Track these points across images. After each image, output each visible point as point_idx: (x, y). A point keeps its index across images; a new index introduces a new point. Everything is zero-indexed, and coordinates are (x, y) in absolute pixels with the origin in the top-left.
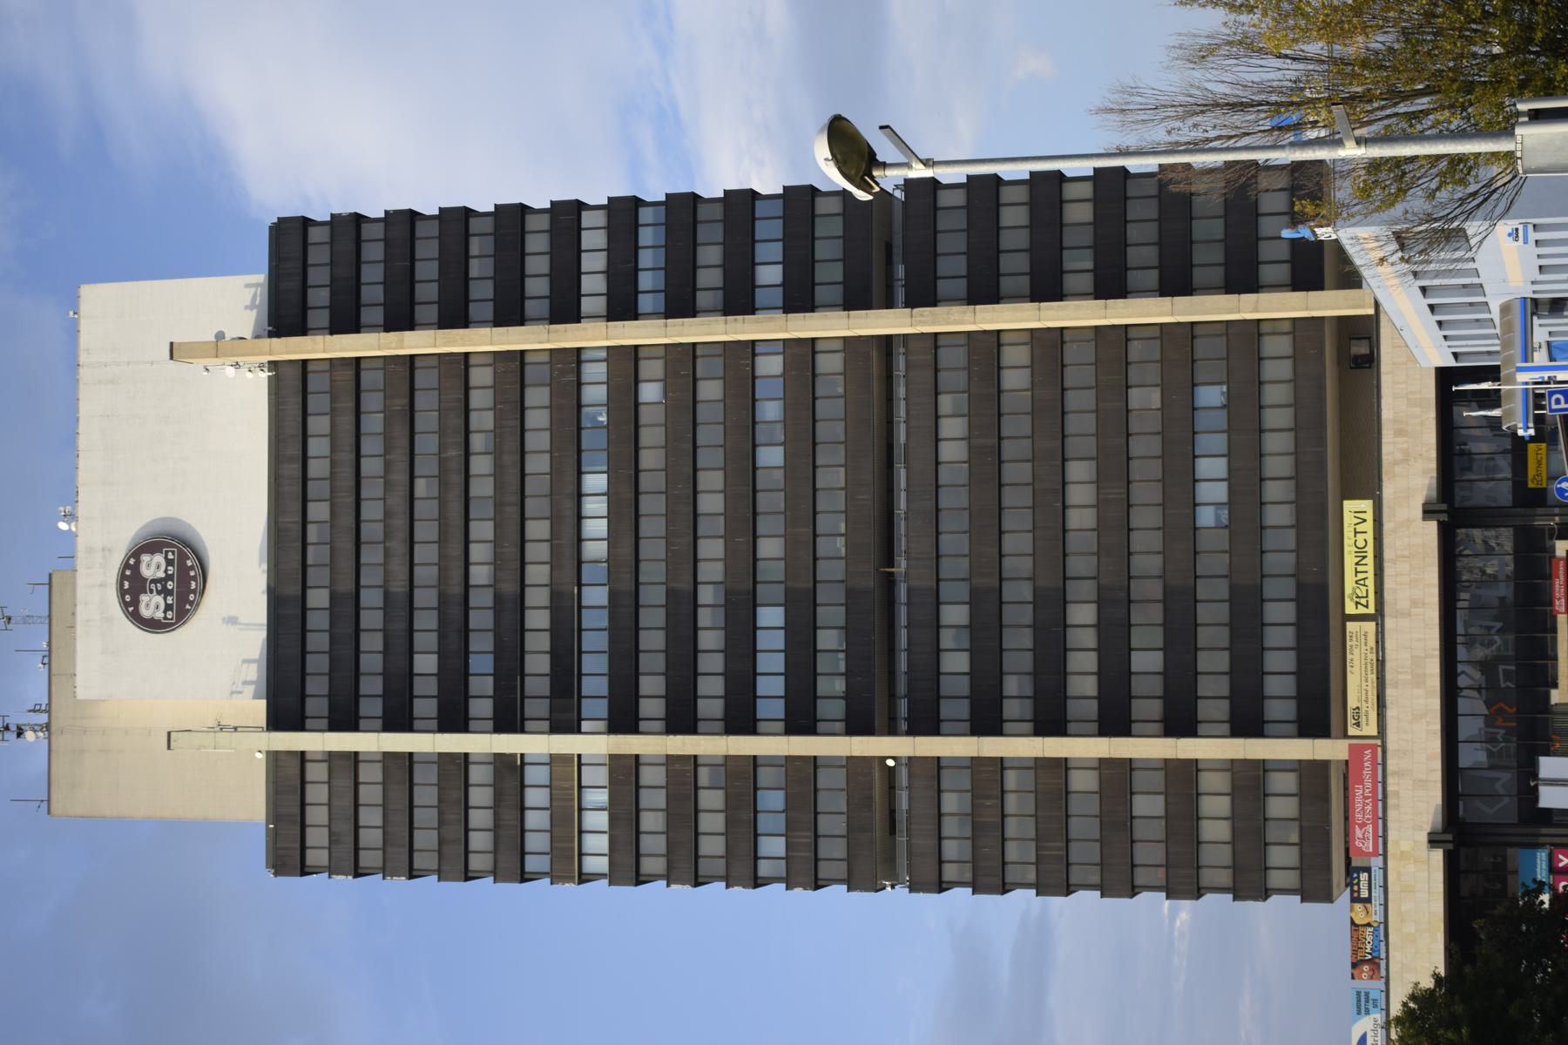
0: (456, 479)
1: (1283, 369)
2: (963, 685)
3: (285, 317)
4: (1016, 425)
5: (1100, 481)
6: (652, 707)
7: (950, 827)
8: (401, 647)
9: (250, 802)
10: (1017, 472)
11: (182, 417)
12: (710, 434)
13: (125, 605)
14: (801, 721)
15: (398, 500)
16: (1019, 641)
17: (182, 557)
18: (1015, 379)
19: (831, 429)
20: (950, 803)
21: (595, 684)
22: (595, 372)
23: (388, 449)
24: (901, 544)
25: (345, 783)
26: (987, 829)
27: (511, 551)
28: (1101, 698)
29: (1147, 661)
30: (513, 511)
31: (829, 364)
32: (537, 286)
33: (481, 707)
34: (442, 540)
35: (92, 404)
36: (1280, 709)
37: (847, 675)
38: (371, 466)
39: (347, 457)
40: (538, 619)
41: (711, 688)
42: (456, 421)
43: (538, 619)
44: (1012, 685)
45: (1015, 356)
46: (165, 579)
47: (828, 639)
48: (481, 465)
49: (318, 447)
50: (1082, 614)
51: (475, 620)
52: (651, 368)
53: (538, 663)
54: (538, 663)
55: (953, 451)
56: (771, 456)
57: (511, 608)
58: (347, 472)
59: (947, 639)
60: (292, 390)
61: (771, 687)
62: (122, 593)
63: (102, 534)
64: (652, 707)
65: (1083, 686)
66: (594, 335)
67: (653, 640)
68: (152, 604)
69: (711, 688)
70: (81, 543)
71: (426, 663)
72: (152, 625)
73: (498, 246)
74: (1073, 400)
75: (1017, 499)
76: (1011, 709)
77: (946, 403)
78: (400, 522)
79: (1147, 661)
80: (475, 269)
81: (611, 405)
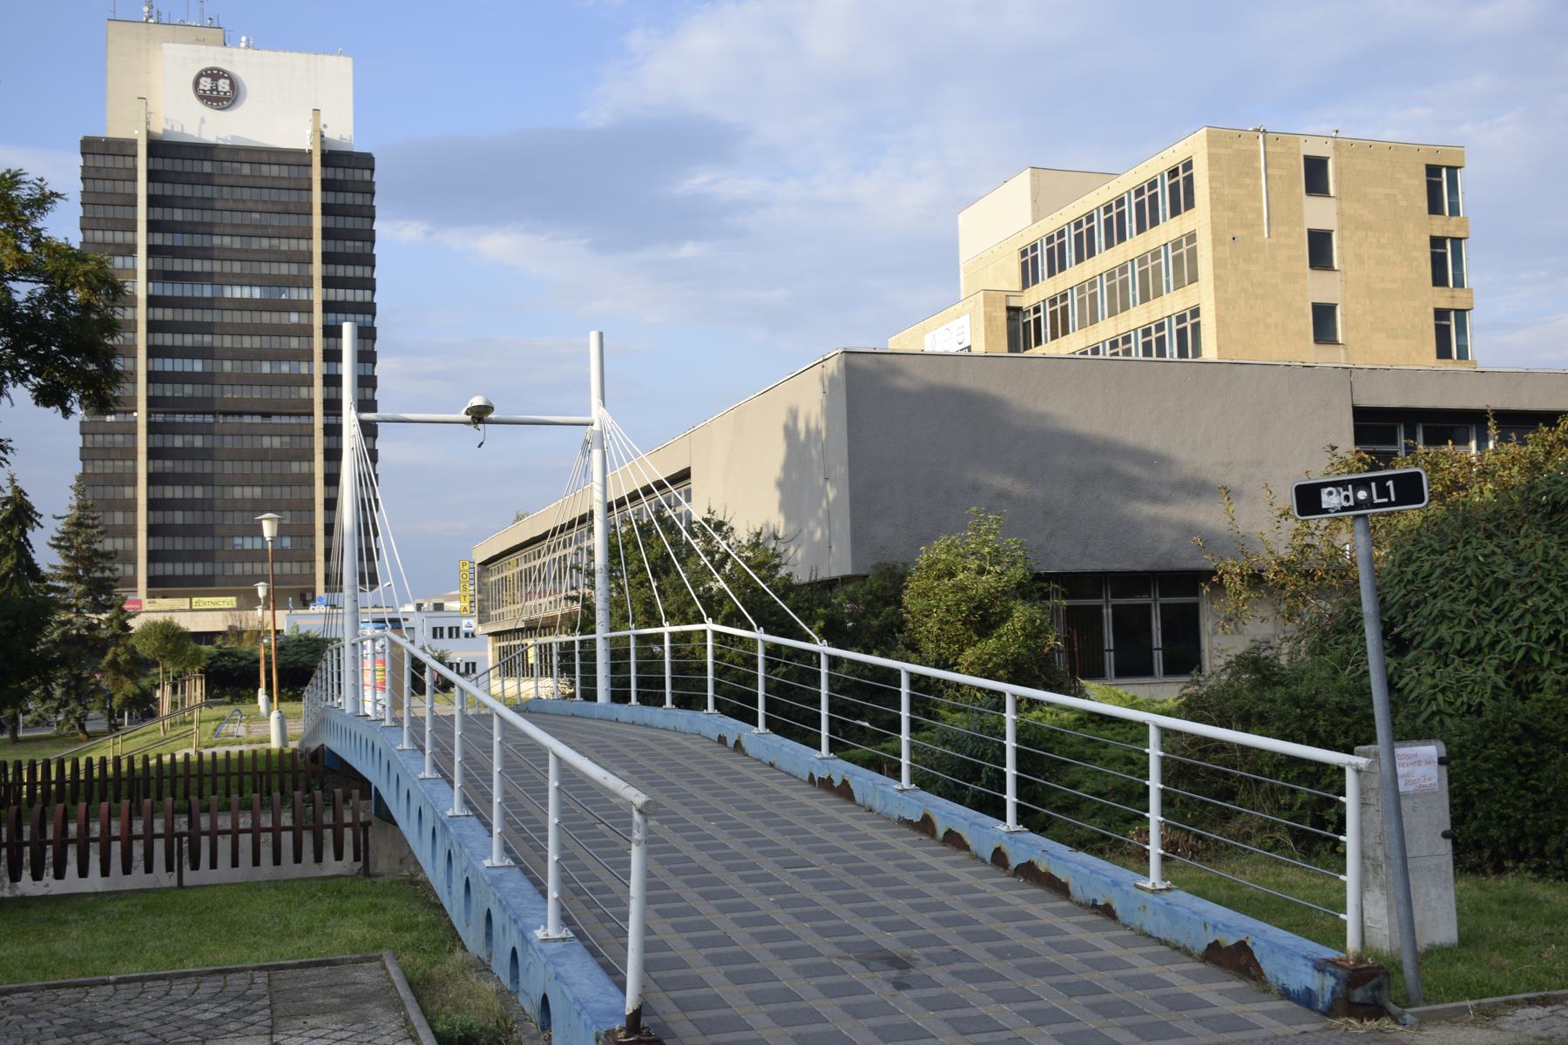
0: (259, 232)
1: (296, 570)
2: (168, 444)
3: (332, 158)
4: (276, 468)
5: (253, 500)
6: (159, 314)
7: (109, 438)
8: (185, 203)
9: (116, 129)
10: (258, 467)
11: (291, 104)
12: (276, 343)
13: (206, 70)
14: (152, 377)
15: (250, 205)
16: (187, 467)
17: (228, 100)
18: (295, 467)
19: (276, 393)
20: (119, 438)
21: (168, 290)
22: (303, 294)
23: (273, 202)
24: (230, 419)
25: (124, 175)
26: (107, 453)
27: (227, 255)
28: (163, 499)
29: (179, 517)
30: (244, 256)
31: (304, 392)
32: (341, 271)
33: (158, 239)
34: (233, 225)
35: (298, 60)
36: (159, 569)
37: (173, 397)
38: (265, 194)
39: (269, 184)
40: (198, 266)
41: (167, 339)
42: (284, 233)
43: (198, 266)
44: (169, 464)
45: (305, 466)
46: (218, 90)
47: (188, 389)
48: (265, 243)
49: (275, 170)
50: (198, 492)
51: (197, 238)
52: (304, 318)
53: (178, 265)
54: (178, 265)
55: (266, 442)
56: (266, 367)
57: (206, 254)
58: (263, 183)
59: (188, 438)
60: (299, 159)
61: (168, 365)
62: (212, 69)
63: (239, 61)
64: (159, 314)
65: (170, 492)
66: (317, 294)
67: (188, 315)
68: (206, 83)
69: (167, 339)
70: (235, 50)
71: (178, 215)
72: (196, 83)
73: (358, 255)
74: (286, 490)
75: (246, 467)
76: (159, 463)
77: (287, 439)
78: (240, 206)
79: (179, 517)
80: (349, 243)
81: (289, 301)
